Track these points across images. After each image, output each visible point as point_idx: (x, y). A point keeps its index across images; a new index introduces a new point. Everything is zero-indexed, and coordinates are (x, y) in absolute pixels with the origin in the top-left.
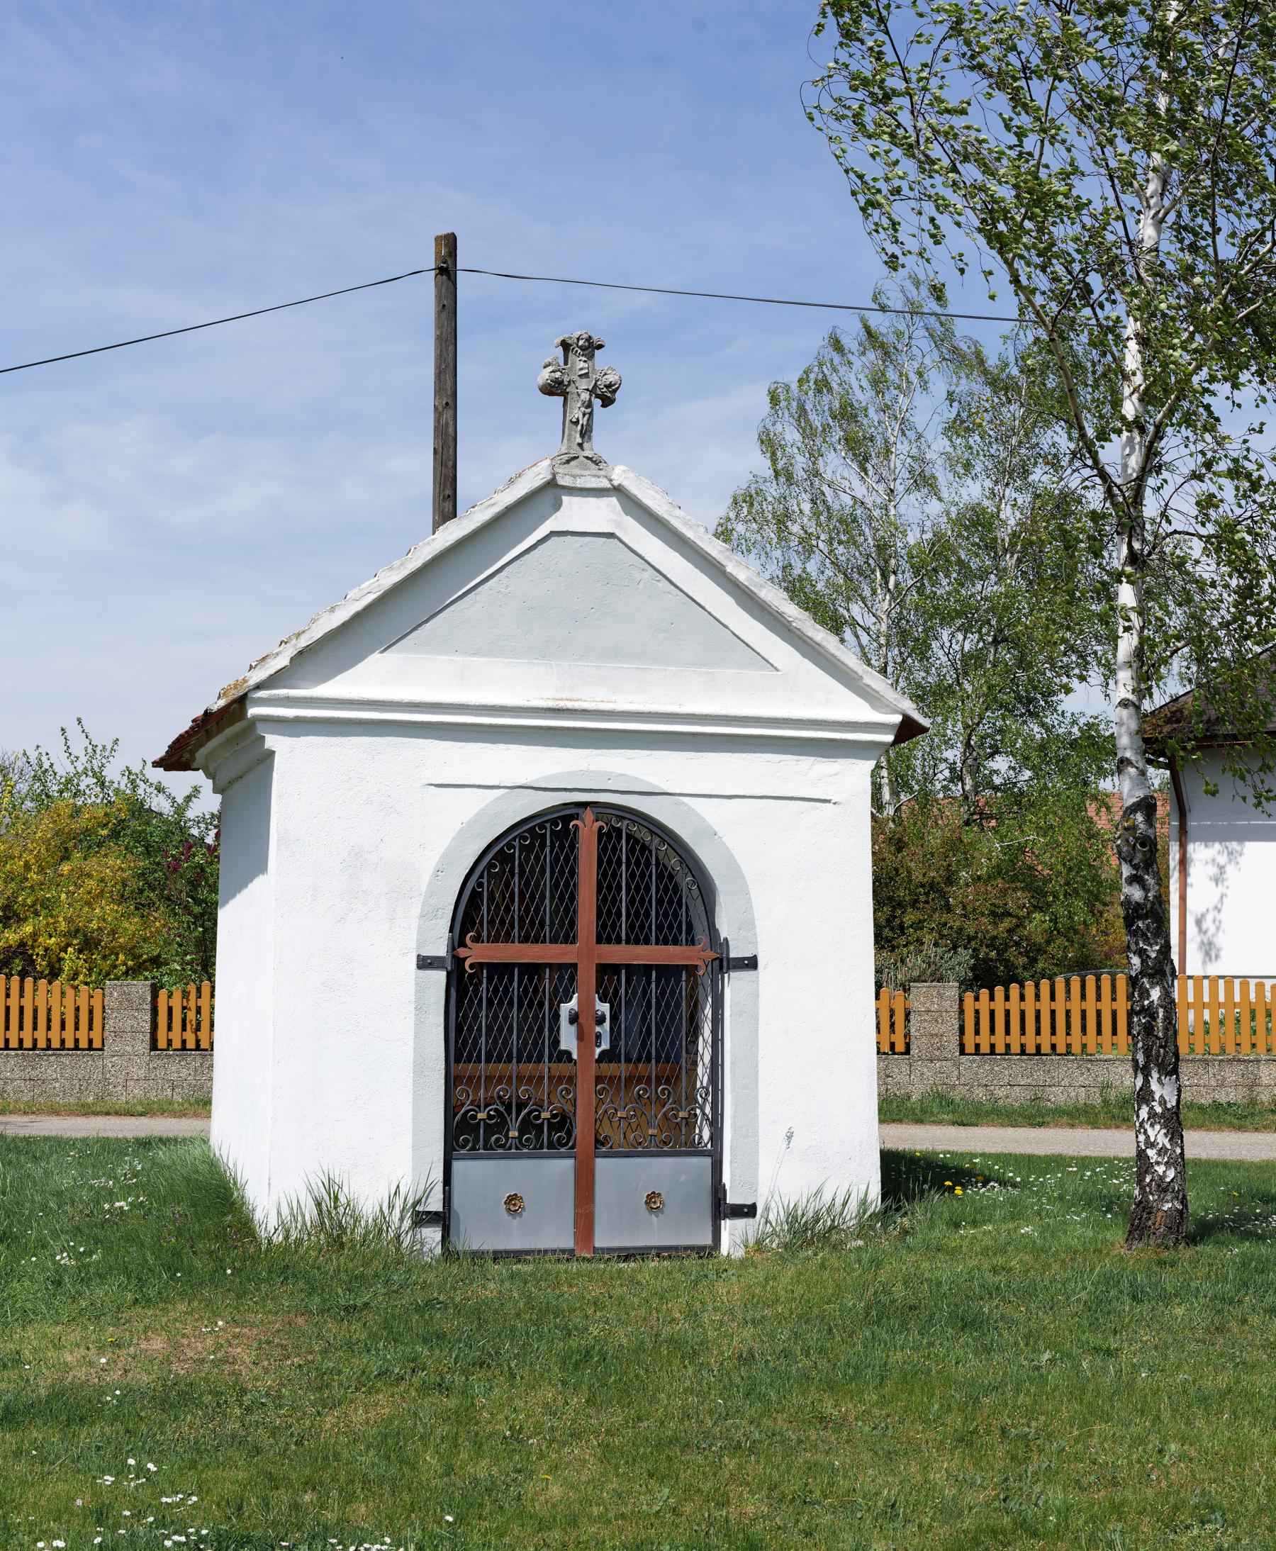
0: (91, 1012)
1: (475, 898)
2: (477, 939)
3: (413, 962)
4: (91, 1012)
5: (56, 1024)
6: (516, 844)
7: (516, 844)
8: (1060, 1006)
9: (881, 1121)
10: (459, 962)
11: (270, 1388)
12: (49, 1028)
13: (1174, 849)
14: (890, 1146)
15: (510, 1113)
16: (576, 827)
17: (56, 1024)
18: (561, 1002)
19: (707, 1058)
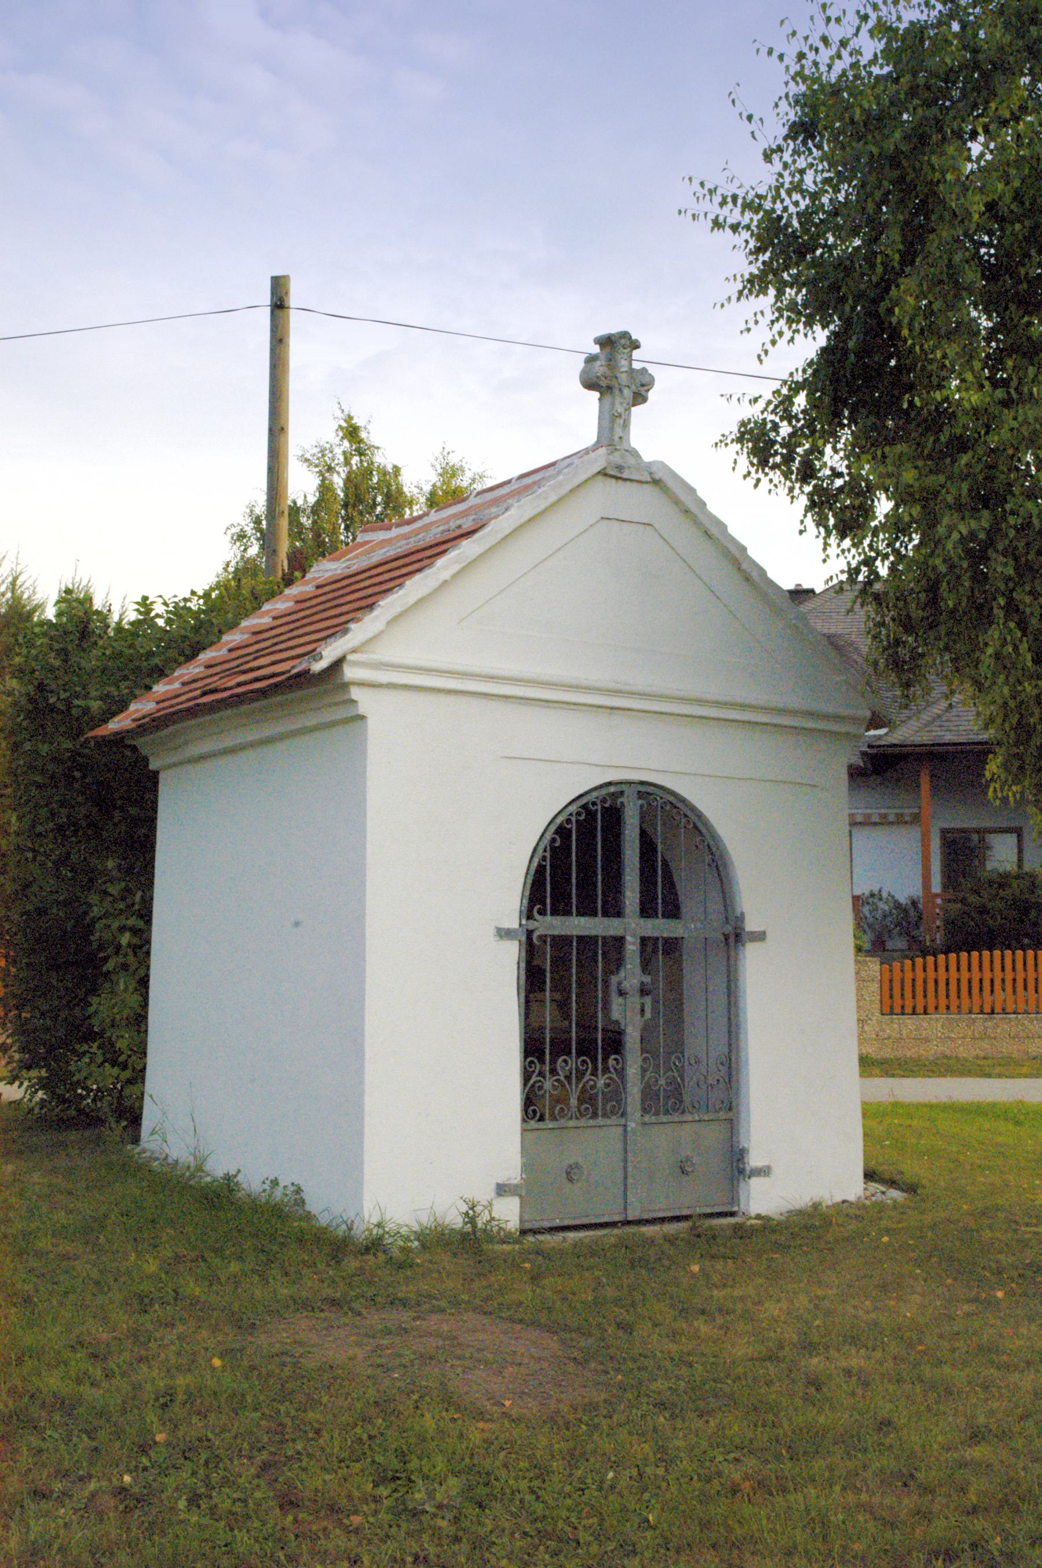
0: (981, 989)
1: (540, 870)
2: (542, 913)
3: (492, 931)
4: (981, 989)
5: (987, 984)
6: (574, 819)
7: (574, 819)
8: (976, 976)
9: (861, 1076)
10: (530, 933)
11: (941, 652)
12: (981, 980)
13: (936, 887)
14: (866, 1100)
15: (570, 1084)
16: (622, 803)
17: (987, 984)
18: (612, 973)
19: (293, 727)
